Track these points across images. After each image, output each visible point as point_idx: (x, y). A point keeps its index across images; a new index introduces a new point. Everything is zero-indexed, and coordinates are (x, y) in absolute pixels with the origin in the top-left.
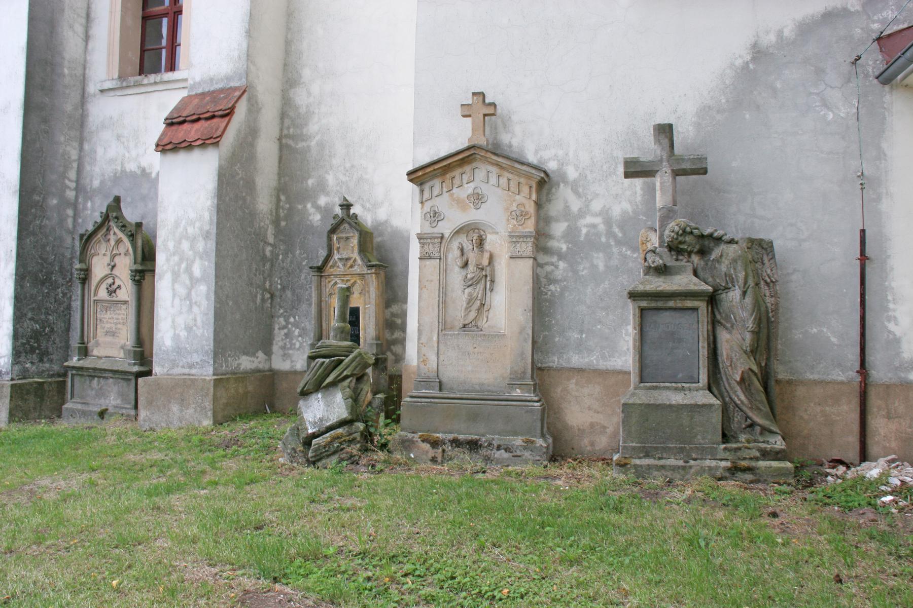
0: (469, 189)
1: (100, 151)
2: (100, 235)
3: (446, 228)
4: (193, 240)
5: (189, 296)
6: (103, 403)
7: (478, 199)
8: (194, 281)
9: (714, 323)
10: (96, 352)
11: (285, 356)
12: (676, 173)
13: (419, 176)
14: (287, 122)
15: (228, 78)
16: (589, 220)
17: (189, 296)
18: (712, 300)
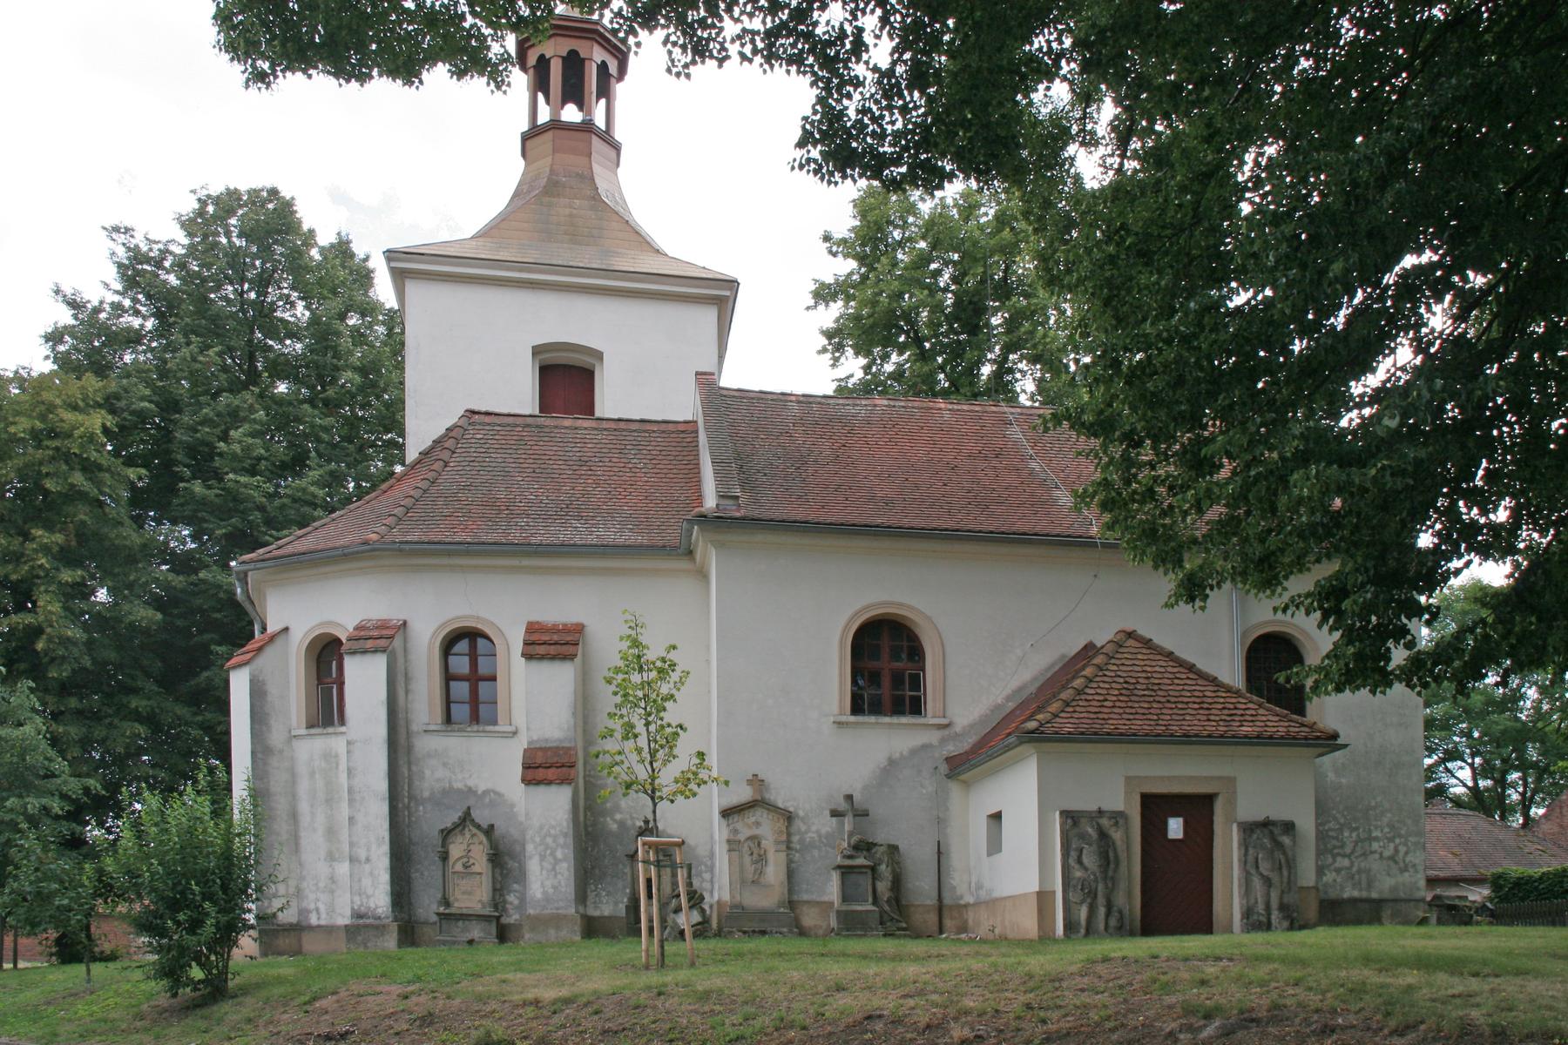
0: (753, 819)
1: (428, 773)
2: (457, 830)
3: (742, 837)
4: (555, 838)
5: (554, 869)
6: (469, 936)
7: (758, 824)
8: (557, 861)
9: (874, 879)
10: (456, 905)
11: (596, 908)
12: (855, 816)
13: (726, 813)
14: (588, 768)
15: (561, 741)
16: (810, 835)
17: (554, 869)
18: (873, 869)
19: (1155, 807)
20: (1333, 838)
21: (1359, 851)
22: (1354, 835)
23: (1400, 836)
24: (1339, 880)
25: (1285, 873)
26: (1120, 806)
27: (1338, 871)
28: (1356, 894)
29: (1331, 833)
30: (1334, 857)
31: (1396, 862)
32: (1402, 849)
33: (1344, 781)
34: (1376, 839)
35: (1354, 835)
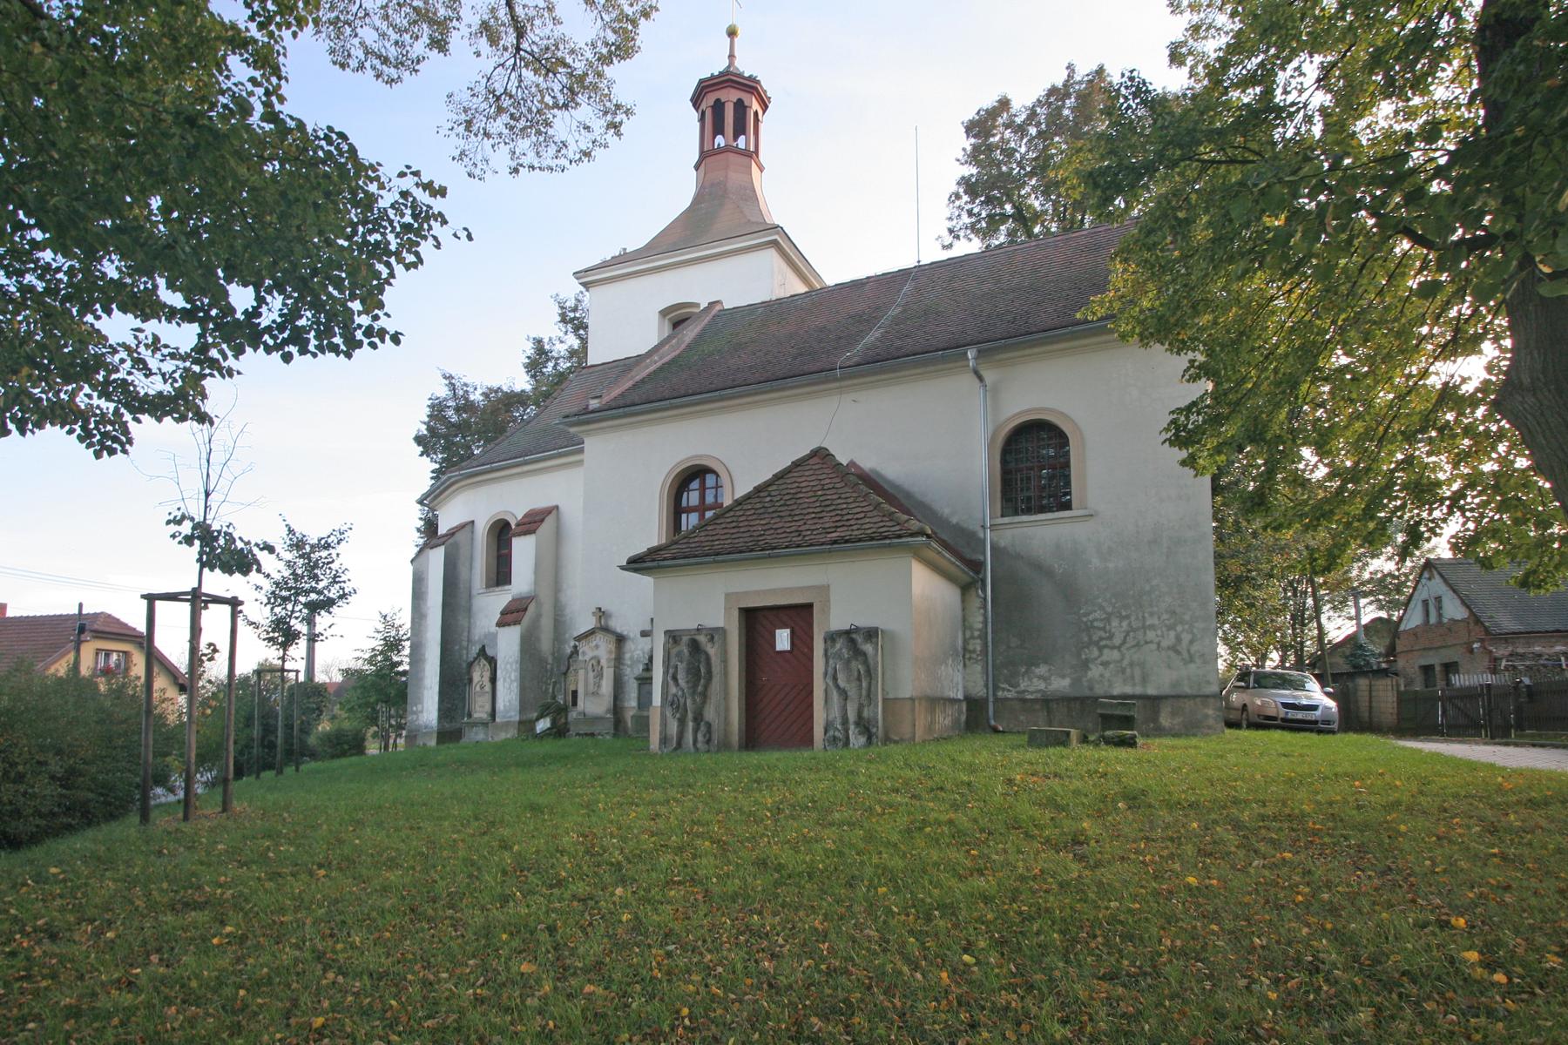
19: (755, 621)
20: (1099, 629)
21: (1131, 642)
22: (1125, 624)
23: (1182, 622)
24: (1107, 675)
25: (864, 684)
26: (721, 624)
27: (1105, 664)
28: (1128, 690)
29: (1096, 624)
30: (1101, 649)
31: (1178, 653)
32: (1186, 637)
33: (1111, 565)
34: (1152, 627)
35: (1125, 624)
